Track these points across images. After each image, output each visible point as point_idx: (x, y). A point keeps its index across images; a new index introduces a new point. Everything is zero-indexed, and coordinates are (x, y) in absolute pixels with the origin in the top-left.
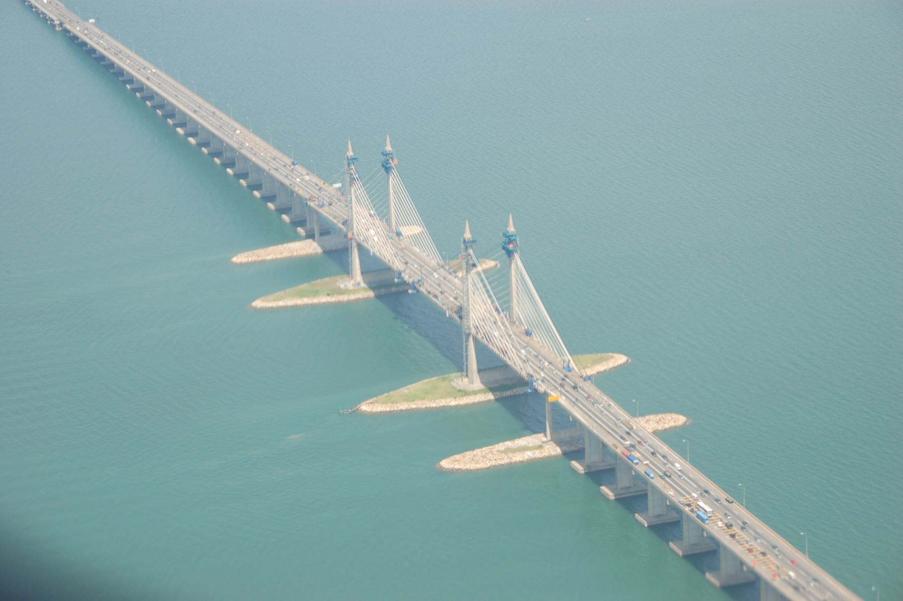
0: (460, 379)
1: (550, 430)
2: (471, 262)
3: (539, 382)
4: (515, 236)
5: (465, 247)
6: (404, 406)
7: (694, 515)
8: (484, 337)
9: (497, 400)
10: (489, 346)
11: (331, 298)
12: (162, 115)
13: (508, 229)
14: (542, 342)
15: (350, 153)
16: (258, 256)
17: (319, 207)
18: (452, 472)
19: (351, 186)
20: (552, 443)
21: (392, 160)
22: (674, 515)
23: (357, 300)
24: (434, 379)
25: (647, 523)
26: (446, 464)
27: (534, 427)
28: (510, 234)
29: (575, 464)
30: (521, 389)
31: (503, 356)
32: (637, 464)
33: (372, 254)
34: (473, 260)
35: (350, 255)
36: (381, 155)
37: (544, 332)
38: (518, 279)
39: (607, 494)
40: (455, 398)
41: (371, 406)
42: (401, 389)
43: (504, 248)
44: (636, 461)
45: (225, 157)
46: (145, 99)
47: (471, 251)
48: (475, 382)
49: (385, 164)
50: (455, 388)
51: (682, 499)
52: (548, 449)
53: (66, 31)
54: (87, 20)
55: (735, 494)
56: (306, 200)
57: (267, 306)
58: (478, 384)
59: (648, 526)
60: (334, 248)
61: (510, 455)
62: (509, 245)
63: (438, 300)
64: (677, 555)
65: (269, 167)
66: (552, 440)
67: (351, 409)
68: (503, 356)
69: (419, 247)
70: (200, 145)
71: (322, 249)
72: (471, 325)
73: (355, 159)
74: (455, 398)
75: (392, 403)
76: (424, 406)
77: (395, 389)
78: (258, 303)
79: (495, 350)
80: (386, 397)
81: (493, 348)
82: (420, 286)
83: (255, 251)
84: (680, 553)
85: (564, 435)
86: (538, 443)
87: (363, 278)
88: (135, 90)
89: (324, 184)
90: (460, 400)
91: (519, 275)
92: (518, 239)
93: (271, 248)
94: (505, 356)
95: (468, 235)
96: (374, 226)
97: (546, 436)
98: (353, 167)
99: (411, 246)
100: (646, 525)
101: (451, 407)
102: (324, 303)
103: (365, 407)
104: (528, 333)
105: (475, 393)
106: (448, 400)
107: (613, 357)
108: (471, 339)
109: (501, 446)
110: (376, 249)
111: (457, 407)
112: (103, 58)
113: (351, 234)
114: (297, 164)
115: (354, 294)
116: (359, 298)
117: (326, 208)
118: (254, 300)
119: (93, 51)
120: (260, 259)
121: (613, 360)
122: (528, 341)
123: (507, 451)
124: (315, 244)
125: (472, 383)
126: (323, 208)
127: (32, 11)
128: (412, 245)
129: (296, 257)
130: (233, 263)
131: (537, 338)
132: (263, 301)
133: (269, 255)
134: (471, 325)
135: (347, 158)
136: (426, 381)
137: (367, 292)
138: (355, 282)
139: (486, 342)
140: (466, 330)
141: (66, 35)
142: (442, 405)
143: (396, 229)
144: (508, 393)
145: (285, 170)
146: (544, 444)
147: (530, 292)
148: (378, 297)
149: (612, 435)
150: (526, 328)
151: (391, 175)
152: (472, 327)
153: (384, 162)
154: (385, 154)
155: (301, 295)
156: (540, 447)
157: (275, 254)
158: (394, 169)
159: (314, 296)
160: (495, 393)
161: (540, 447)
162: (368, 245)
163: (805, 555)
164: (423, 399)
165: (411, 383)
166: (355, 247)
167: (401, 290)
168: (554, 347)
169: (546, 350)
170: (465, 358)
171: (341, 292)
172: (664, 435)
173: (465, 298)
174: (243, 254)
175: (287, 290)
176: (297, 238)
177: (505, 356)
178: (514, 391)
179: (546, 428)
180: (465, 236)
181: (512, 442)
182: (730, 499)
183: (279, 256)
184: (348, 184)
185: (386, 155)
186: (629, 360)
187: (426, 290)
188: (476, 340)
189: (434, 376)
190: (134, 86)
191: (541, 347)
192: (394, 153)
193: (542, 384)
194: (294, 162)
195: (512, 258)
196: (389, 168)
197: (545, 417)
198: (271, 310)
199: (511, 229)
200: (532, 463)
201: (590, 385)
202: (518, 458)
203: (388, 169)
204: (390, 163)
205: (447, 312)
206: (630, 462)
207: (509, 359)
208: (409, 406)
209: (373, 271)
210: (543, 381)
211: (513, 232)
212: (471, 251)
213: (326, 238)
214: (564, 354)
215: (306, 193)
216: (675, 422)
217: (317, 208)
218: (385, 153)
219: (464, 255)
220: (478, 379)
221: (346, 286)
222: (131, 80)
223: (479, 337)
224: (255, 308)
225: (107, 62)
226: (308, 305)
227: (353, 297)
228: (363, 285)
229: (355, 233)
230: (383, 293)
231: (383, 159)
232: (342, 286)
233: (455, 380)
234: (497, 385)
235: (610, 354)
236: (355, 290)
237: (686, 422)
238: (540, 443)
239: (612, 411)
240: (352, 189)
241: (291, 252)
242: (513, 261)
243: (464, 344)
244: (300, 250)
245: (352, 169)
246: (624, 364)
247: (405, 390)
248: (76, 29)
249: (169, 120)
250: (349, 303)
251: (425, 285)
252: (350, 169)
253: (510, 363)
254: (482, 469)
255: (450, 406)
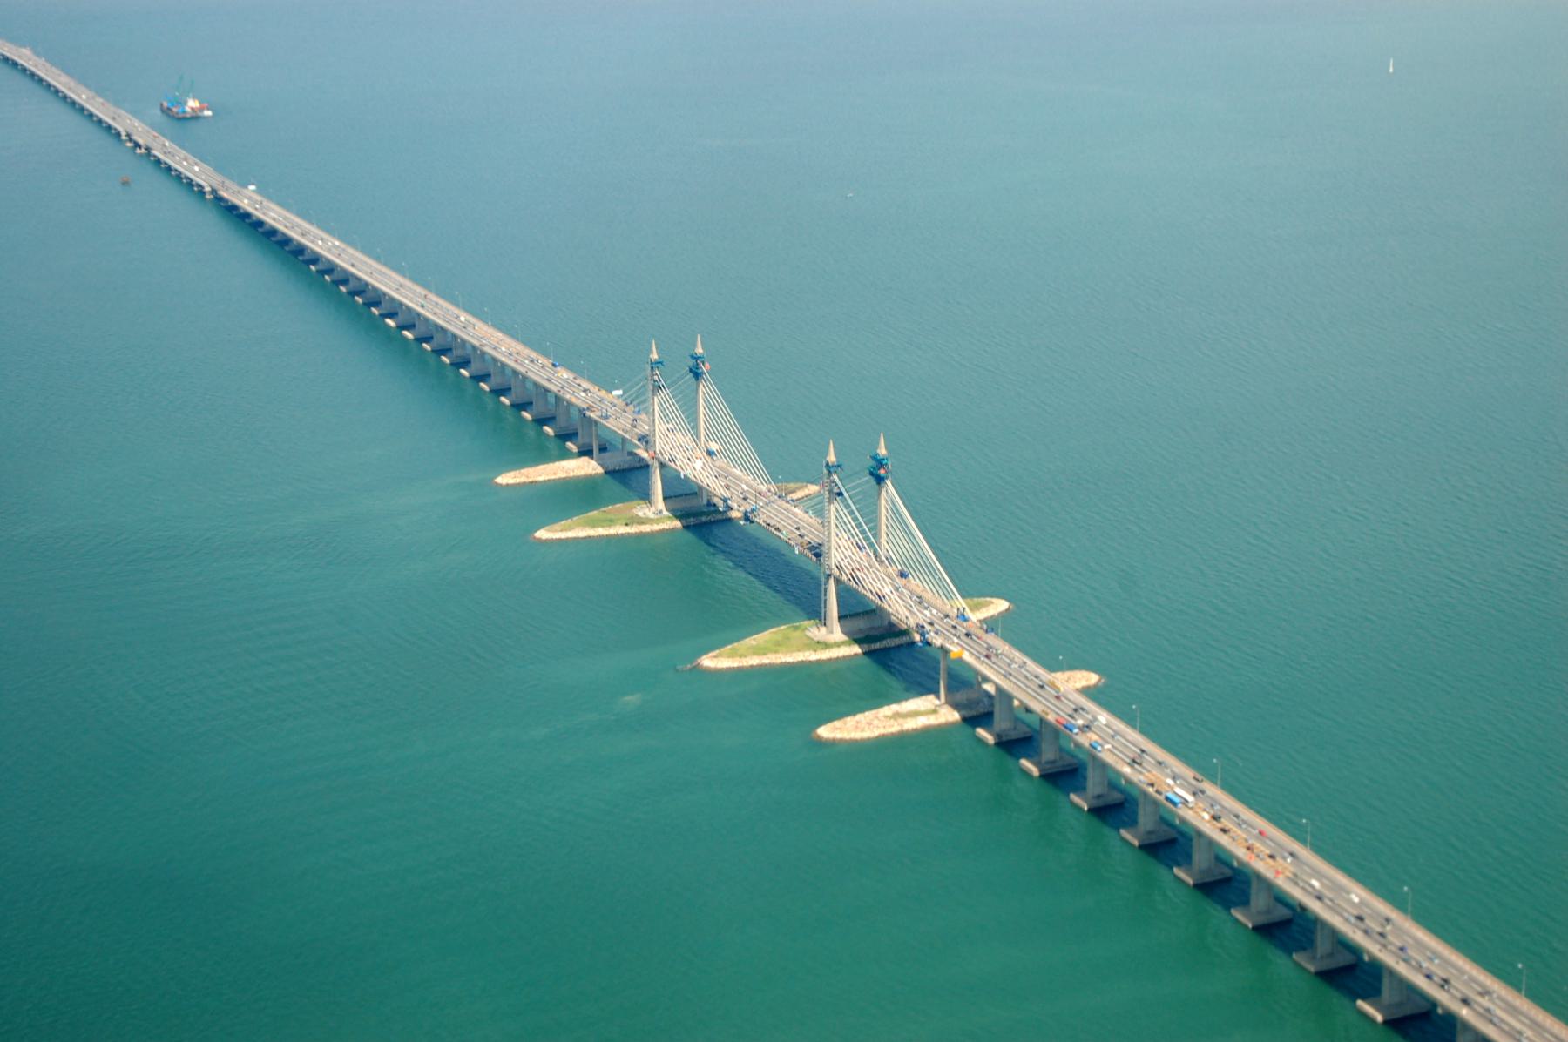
2: (836, 490)
3: (932, 634)
6: (754, 661)
7: (1161, 798)
9: (865, 653)
15: (655, 356)
18: (833, 743)
19: (654, 395)
20: (946, 706)
24: (783, 627)
26: (825, 732)
28: (881, 457)
29: (981, 732)
31: (880, 602)
32: (1077, 734)
33: (682, 477)
36: (689, 358)
41: (715, 660)
46: (337, 283)
47: (835, 477)
48: (835, 631)
50: (812, 639)
51: (1141, 778)
54: (245, 186)
56: (584, 409)
57: (554, 537)
58: (838, 634)
59: (1089, 810)
60: (617, 468)
61: (901, 721)
62: (879, 469)
64: (1131, 845)
68: (880, 602)
71: (603, 468)
76: (778, 661)
77: (739, 639)
78: (542, 534)
82: (755, 516)
83: (522, 471)
85: (961, 696)
87: (665, 505)
97: (938, 697)
99: (728, 468)
100: (1086, 808)
103: (708, 662)
104: (902, 575)
105: (838, 645)
106: (807, 653)
107: (992, 603)
109: (887, 710)
110: (689, 471)
111: (818, 662)
116: (664, 529)
118: (539, 529)
119: (260, 223)
120: (531, 480)
121: (992, 606)
123: (897, 715)
124: (593, 463)
125: (832, 632)
129: (570, 478)
131: (915, 580)
132: (549, 531)
136: (774, 630)
139: (854, 585)
141: (220, 205)
143: (706, 447)
144: (877, 646)
146: (938, 708)
148: (686, 527)
152: (834, 567)
154: (696, 358)
156: (934, 711)
159: (610, 526)
161: (934, 711)
163: (1306, 846)
165: (757, 633)
167: (713, 519)
168: (940, 592)
170: (823, 602)
171: (642, 521)
172: (1086, 691)
174: (508, 474)
176: (565, 455)
178: (884, 642)
179: (939, 689)
180: (828, 459)
182: (1200, 777)
183: (553, 477)
184: (651, 393)
187: (764, 521)
188: (838, 581)
190: (321, 266)
195: (882, 485)
197: (939, 674)
199: (882, 451)
200: (926, 732)
202: (911, 724)
203: (697, 375)
206: (1068, 732)
207: (889, 605)
216: (1087, 680)
221: (645, 514)
223: (844, 578)
224: (540, 540)
225: (279, 237)
227: (656, 527)
228: (665, 513)
229: (658, 452)
232: (640, 514)
235: (988, 599)
236: (657, 519)
237: (1099, 681)
238: (933, 707)
240: (656, 399)
241: (566, 472)
243: (823, 586)
247: (751, 641)
250: (652, 534)
251: (761, 516)
253: (891, 610)
254: (869, 739)
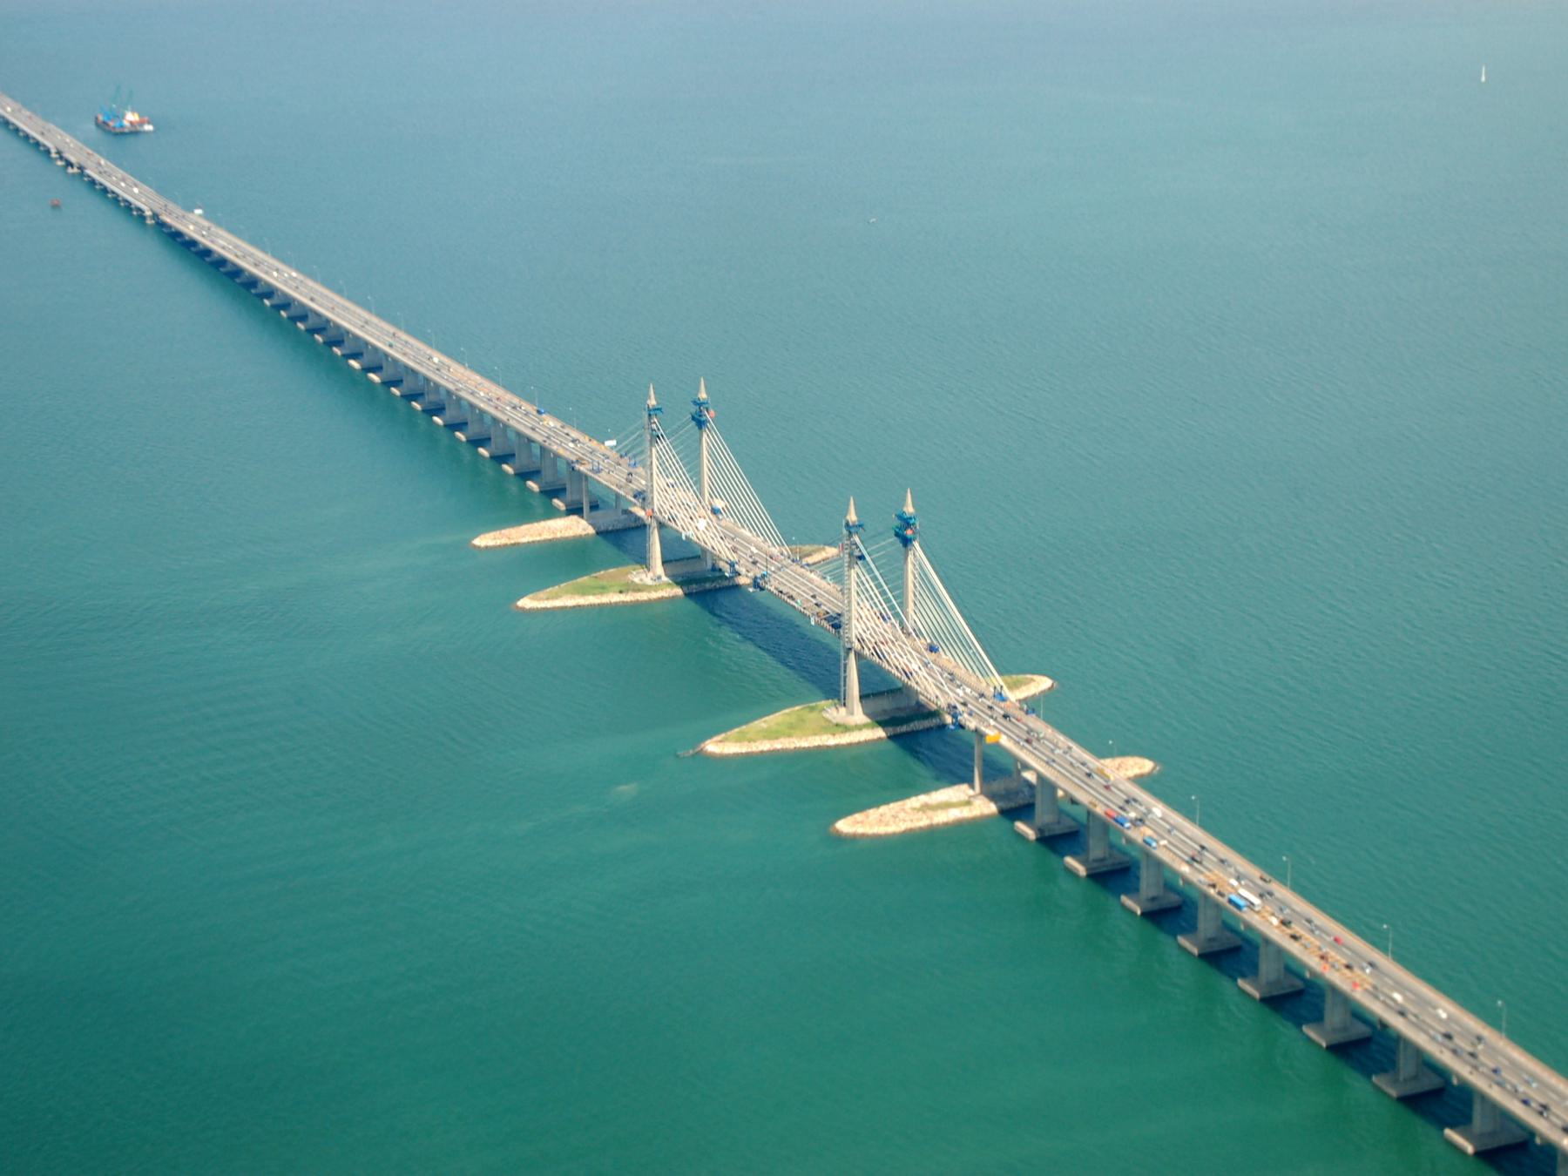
0: (834, 709)
2: (857, 553)
3: (966, 715)
6: (765, 746)
7: (1223, 901)
8: (874, 653)
9: (890, 737)
12: (324, 343)
14: (955, 660)
15: (652, 402)
18: (854, 839)
20: (982, 797)
21: (707, 411)
22: (1173, 899)
23: (661, 600)
24: (797, 708)
25: (1141, 909)
26: (845, 826)
29: (1021, 826)
32: (1128, 828)
33: (684, 538)
34: (860, 551)
37: (957, 644)
39: (1076, 869)
41: (721, 745)
42: (756, 722)
43: (897, 535)
44: (1127, 825)
45: (427, 400)
46: (294, 319)
47: (856, 539)
48: (855, 712)
49: (696, 416)
50: (830, 721)
51: (1202, 878)
52: (979, 806)
53: (161, 225)
54: (191, 210)
55: (1274, 870)
56: (573, 462)
58: (859, 716)
60: (610, 528)
61: (930, 813)
63: (797, 602)
66: (982, 793)
67: (694, 749)
69: (750, 529)
73: (658, 409)
75: (749, 742)
76: (792, 746)
77: (747, 722)
78: (526, 603)
79: (894, 671)
80: (738, 732)
81: (890, 668)
83: (503, 531)
85: (998, 786)
86: (963, 797)
92: (917, 524)
93: (525, 527)
94: (909, 678)
95: (852, 517)
96: (666, 494)
97: (972, 787)
98: (656, 421)
100: (1139, 912)
102: (616, 603)
103: (713, 747)
104: (932, 649)
105: (859, 728)
112: (222, 262)
113: (650, 511)
115: (656, 591)
116: (662, 597)
117: (603, 474)
120: (513, 542)
123: (926, 808)
124: (583, 522)
125: (852, 714)
127: (95, 189)
128: (738, 527)
132: (533, 599)
133: (523, 537)
136: (787, 711)
139: (878, 660)
142: (816, 744)
144: (904, 729)
146: (972, 799)
147: (934, 589)
150: (929, 641)
153: (696, 413)
154: (699, 404)
155: (583, 591)
156: (968, 803)
157: (531, 536)
159: (602, 594)
161: (968, 803)
163: (1388, 955)
164: (790, 736)
170: (842, 679)
173: (846, 602)
175: (562, 585)
177: (909, 678)
178: (912, 725)
180: (848, 518)
182: (1268, 877)
183: (538, 538)
184: (648, 443)
185: (700, 405)
188: (859, 656)
190: (276, 301)
191: (955, 667)
193: (971, 719)
195: (909, 548)
199: (909, 509)
202: (941, 817)
203: (701, 424)
204: (705, 415)
205: (812, 619)
206: (1119, 826)
208: (772, 745)
209: (681, 559)
210: (970, 714)
211: (912, 514)
212: (856, 539)
213: (594, 513)
214: (989, 673)
215: (568, 453)
216: (1140, 768)
220: (860, 709)
221: (641, 580)
223: (866, 652)
226: (594, 605)
227: (654, 595)
228: (665, 579)
229: (656, 510)
230: (694, 591)
232: (636, 580)
234: (887, 717)
235: (1029, 676)
237: (1154, 768)
238: (967, 798)
240: (654, 450)
241: (553, 533)
245: (655, 423)
246: (1049, 689)
247: (762, 724)
248: (188, 228)
250: (650, 602)
252: (651, 423)
254: (894, 834)
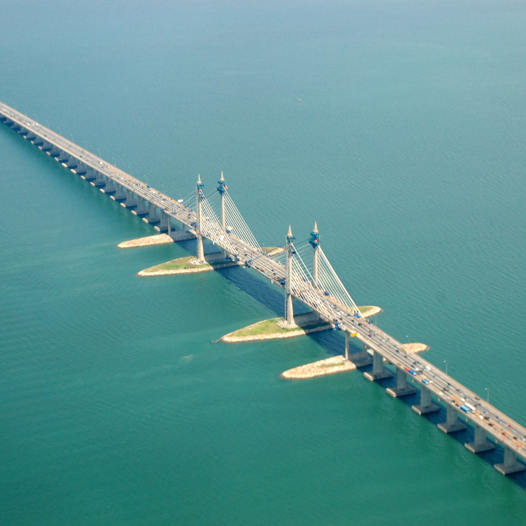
0: (282, 321)
1: (348, 353)
2: (292, 251)
3: (341, 324)
4: (318, 235)
5: (288, 241)
6: (250, 338)
9: (307, 334)
10: (304, 302)
11: (187, 271)
13: (314, 231)
14: (337, 299)
15: (199, 182)
16: (135, 244)
17: (173, 215)
18: (291, 380)
19: (199, 202)
20: (349, 361)
21: (224, 186)
23: (203, 272)
24: (265, 321)
25: (421, 412)
26: (287, 374)
27: (339, 352)
28: (315, 234)
29: (366, 374)
30: (321, 327)
32: (415, 375)
33: (214, 244)
34: (294, 249)
35: (197, 244)
37: (333, 293)
38: (319, 259)
40: (282, 333)
41: (231, 338)
42: (247, 327)
43: (310, 242)
46: (37, 145)
47: (292, 244)
49: (220, 189)
50: (280, 327)
51: (448, 398)
55: (482, 395)
56: (163, 209)
58: (293, 324)
59: (422, 414)
60: (180, 239)
61: (325, 369)
62: (314, 240)
63: (265, 273)
64: (443, 432)
65: (134, 189)
66: (349, 359)
67: (218, 340)
70: (80, 174)
71: (173, 239)
72: (291, 288)
73: (202, 185)
74: (282, 333)
76: (263, 338)
78: (142, 273)
79: (309, 304)
81: (307, 303)
82: (251, 264)
83: (132, 241)
84: (446, 431)
85: (356, 356)
88: (30, 139)
89: (171, 199)
90: (285, 334)
91: (320, 257)
93: (142, 239)
97: (345, 357)
99: (237, 239)
100: (420, 413)
101: (279, 338)
102: (183, 273)
103: (227, 338)
104: (326, 294)
105: (293, 330)
106: (278, 334)
107: (372, 308)
108: (290, 297)
111: (283, 339)
113: (199, 231)
114: (151, 187)
115: (201, 268)
117: (177, 215)
121: (372, 310)
122: (328, 299)
123: (323, 366)
124: (168, 237)
125: (290, 323)
126: (175, 215)
128: (238, 239)
129: (156, 244)
130: (119, 247)
132: (145, 271)
133: (141, 243)
134: (291, 288)
135: (198, 185)
136: (260, 322)
137: (209, 267)
138: (200, 261)
140: (287, 292)
144: (313, 330)
145: (138, 187)
146: (344, 362)
148: (216, 270)
149: (397, 359)
151: (224, 195)
152: (291, 290)
153: (219, 187)
154: (220, 183)
155: (168, 268)
156: (343, 364)
157: (145, 243)
158: (225, 191)
159: (176, 269)
160: (305, 330)
161: (343, 364)
162: (211, 238)
164: (262, 333)
165: (252, 324)
166: (200, 239)
167: (229, 266)
169: (340, 304)
171: (193, 267)
178: (317, 329)
179: (345, 352)
181: (325, 361)
182: (478, 398)
183: (148, 244)
184: (198, 201)
186: (382, 310)
188: (293, 297)
189: (265, 319)
190: (29, 136)
191: (336, 302)
192: (225, 182)
193: (344, 326)
194: (148, 185)
195: (316, 248)
196: (223, 191)
197: (345, 345)
198: (151, 277)
199: (316, 231)
200: (338, 374)
201: (373, 326)
203: (221, 192)
204: (223, 188)
207: (319, 310)
208: (253, 338)
211: (317, 233)
215: (161, 205)
216: (421, 348)
217: (171, 215)
218: (221, 182)
219: (288, 247)
222: (26, 132)
223: (296, 295)
224: (141, 276)
226: (173, 274)
227: (200, 270)
228: (205, 262)
229: (201, 231)
231: (219, 186)
232: (192, 263)
233: (279, 322)
234: (305, 325)
235: (370, 306)
237: (427, 348)
238: (342, 362)
239: (390, 342)
240: (200, 204)
241: (155, 242)
242: (316, 250)
244: (160, 240)
245: (200, 192)
246: (379, 312)
247: (249, 328)
249: (56, 158)
254: (309, 378)
255: (279, 338)
